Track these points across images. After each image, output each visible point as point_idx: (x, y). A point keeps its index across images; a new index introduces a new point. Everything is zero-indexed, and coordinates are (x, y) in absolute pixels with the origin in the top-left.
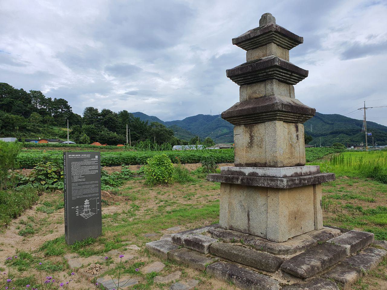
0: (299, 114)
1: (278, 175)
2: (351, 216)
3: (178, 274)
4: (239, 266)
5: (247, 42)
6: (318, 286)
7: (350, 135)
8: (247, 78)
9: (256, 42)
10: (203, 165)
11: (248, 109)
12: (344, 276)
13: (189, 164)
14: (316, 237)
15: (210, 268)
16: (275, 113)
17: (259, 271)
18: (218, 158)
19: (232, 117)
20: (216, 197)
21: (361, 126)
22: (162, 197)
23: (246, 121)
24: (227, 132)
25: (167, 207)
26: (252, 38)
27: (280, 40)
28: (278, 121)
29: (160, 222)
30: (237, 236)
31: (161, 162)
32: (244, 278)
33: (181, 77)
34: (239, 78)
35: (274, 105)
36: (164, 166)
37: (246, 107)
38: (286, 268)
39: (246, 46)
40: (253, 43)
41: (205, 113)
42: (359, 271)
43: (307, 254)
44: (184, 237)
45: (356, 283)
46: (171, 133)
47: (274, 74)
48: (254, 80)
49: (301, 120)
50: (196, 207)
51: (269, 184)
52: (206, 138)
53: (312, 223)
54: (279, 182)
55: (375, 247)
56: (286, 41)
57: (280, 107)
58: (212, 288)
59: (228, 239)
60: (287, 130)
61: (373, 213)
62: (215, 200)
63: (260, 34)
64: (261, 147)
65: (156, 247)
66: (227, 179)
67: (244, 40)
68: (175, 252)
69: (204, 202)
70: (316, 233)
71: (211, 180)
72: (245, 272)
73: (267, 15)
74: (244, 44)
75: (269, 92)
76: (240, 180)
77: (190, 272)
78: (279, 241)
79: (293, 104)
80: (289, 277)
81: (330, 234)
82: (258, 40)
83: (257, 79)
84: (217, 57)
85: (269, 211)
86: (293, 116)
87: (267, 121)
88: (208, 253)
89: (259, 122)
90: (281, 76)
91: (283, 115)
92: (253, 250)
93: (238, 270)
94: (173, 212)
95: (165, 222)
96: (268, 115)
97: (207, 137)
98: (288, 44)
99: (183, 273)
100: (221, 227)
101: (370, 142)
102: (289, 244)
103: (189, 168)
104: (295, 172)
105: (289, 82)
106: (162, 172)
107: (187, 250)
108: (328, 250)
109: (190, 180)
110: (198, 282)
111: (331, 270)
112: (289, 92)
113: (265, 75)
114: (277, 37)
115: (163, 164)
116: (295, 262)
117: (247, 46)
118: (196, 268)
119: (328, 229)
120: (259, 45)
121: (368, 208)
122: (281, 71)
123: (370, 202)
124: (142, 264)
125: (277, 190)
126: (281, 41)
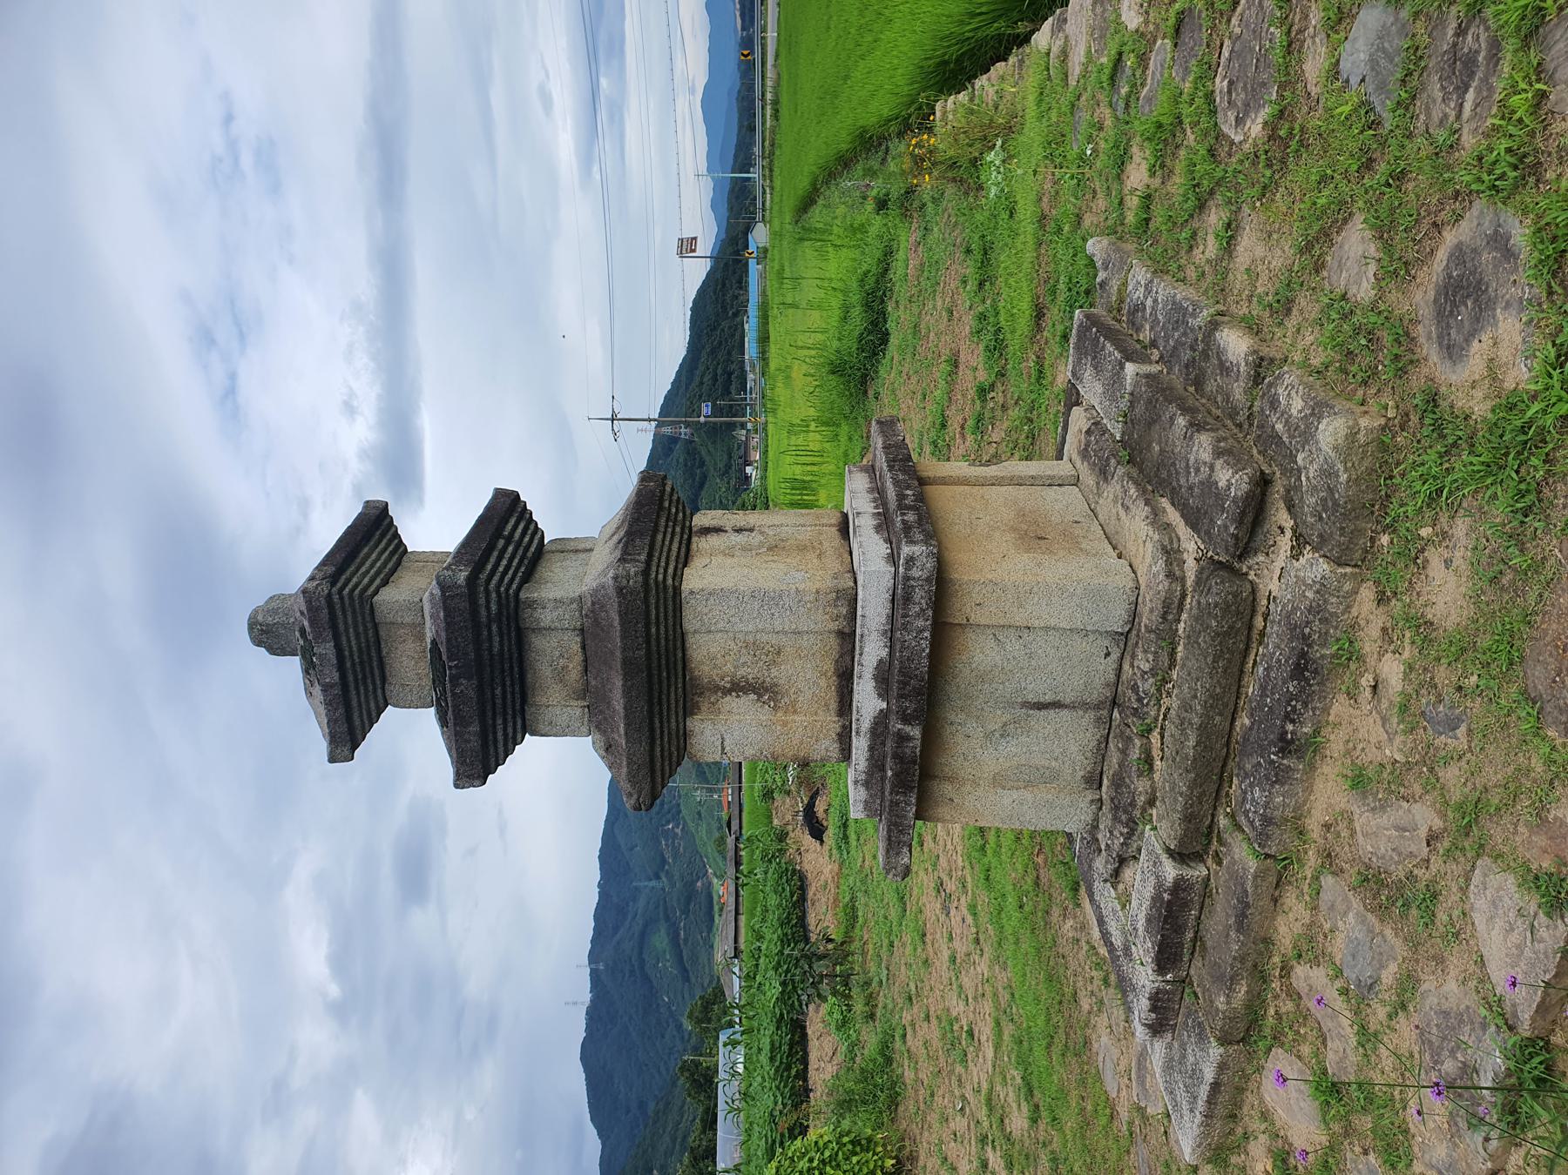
0: (658, 516)
1: (887, 581)
2: (1010, 412)
3: (1307, 978)
4: (1243, 725)
5: (354, 703)
6: (1284, 427)
7: (704, 477)
8: (499, 701)
9: (362, 663)
10: (819, 996)
11: (627, 692)
12: (1235, 362)
13: (812, 1073)
14: (1104, 474)
15: (1263, 837)
17: (1254, 645)
18: (785, 941)
19: (652, 761)
20: (959, 919)
21: (674, 440)
24: (668, 935)
25: (1008, 1130)
26: (343, 676)
27: (368, 572)
28: (684, 583)
29: (1083, 1137)
30: (1124, 752)
32: (1291, 689)
34: (495, 733)
37: (618, 704)
38: (1236, 537)
40: (360, 677)
41: (575, 1029)
42: (1214, 325)
43: (1174, 484)
44: (1145, 977)
45: (1253, 328)
47: (498, 592)
48: (512, 675)
49: (681, 514)
50: (1005, 996)
52: (688, 1026)
53: (1052, 493)
54: (915, 573)
55: (1122, 302)
56: (374, 556)
58: (1345, 816)
59: (1141, 785)
60: (719, 559)
61: (997, 348)
62: (970, 919)
64: (779, 653)
65: (1201, 1104)
66: (902, 784)
67: (341, 710)
68: (1211, 1011)
69: (983, 968)
70: (1089, 479)
71: (906, 859)
72: (1263, 695)
74: (361, 713)
75: (569, 617)
76: (908, 729)
77: (1287, 929)
78: (1131, 584)
80: (1265, 530)
82: (351, 655)
83: (511, 663)
84: (334, 990)
85: (1019, 618)
87: (678, 622)
88: (1202, 865)
90: (511, 572)
91: (663, 564)
92: (1175, 677)
93: (1261, 722)
94: (1030, 1092)
97: (681, 1025)
98: (385, 549)
99: (1300, 956)
100: (1095, 827)
102: (1141, 549)
103: (830, 1069)
104: (872, 531)
105: (532, 549)
107: (1197, 962)
110: (1330, 877)
111: (1218, 408)
112: (571, 555)
113: (500, 628)
114: (355, 580)
116: (1206, 513)
117: (367, 702)
118: (1272, 904)
119: (1071, 448)
120: (374, 654)
122: (489, 567)
123: (956, 367)
125: (941, 585)
126: (372, 572)
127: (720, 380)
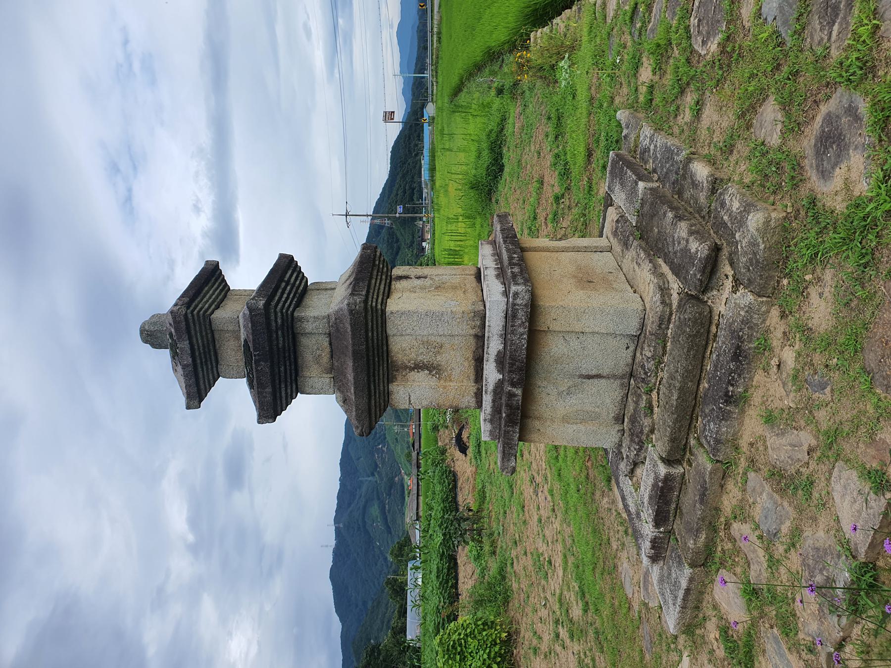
0: (372, 270)
2: (573, 210)
3: (739, 530)
4: (704, 387)
5: (201, 375)
7: (399, 248)
8: (283, 375)
9: (205, 352)
10: (464, 541)
11: (355, 369)
13: (460, 584)
14: (626, 245)
15: (715, 451)
16: (370, 310)
18: (445, 510)
21: (381, 227)
22: (546, 637)
23: (381, 377)
24: (379, 507)
25: (571, 616)
26: (194, 360)
27: (207, 301)
30: (637, 403)
31: (456, 649)
33: (230, 634)
35: (354, 310)
36: (465, 642)
37: (350, 376)
39: (208, 377)
40: (204, 361)
41: (329, 562)
42: (689, 160)
43: (666, 250)
44: (648, 529)
45: (711, 161)
46: (373, 650)
47: (282, 312)
49: (385, 269)
50: (569, 541)
51: (523, 322)
52: (390, 559)
54: (519, 301)
56: (211, 292)
57: (358, 299)
58: (762, 438)
61: (566, 174)
62: (549, 498)
63: (188, 342)
64: (441, 347)
65: (679, 601)
66: (511, 421)
67: (193, 380)
69: (557, 525)
70: (617, 248)
71: (513, 463)
72: (716, 370)
73: (145, 330)
74: (204, 381)
76: (514, 390)
77: (728, 502)
78: (641, 308)
79: (352, 279)
81: (617, 221)
82: (199, 348)
84: (191, 538)
85: (578, 328)
86: (376, 279)
89: (385, 348)
90: (289, 301)
91: (375, 297)
92: (666, 360)
95: (613, 604)
96: (372, 327)
99: (736, 517)
101: (417, 210)
105: (301, 288)
106: (482, 645)
107: (678, 521)
108: (652, 216)
109: (500, 573)
112: (323, 292)
113: (283, 333)
114: (200, 306)
115: (460, 645)
119: (607, 230)
120: (211, 348)
121: (555, 185)
122: (277, 298)
123: (542, 185)
124: (725, 631)
125: (533, 308)
126: (210, 301)
127: (408, 193)
